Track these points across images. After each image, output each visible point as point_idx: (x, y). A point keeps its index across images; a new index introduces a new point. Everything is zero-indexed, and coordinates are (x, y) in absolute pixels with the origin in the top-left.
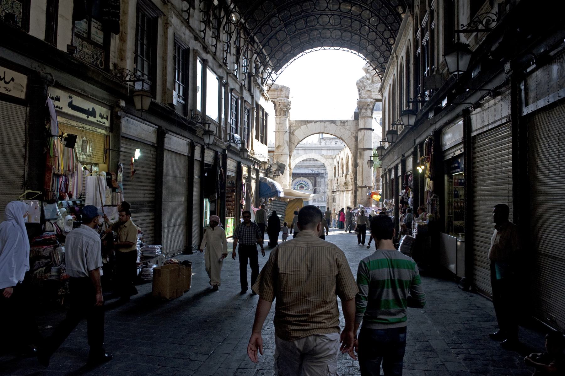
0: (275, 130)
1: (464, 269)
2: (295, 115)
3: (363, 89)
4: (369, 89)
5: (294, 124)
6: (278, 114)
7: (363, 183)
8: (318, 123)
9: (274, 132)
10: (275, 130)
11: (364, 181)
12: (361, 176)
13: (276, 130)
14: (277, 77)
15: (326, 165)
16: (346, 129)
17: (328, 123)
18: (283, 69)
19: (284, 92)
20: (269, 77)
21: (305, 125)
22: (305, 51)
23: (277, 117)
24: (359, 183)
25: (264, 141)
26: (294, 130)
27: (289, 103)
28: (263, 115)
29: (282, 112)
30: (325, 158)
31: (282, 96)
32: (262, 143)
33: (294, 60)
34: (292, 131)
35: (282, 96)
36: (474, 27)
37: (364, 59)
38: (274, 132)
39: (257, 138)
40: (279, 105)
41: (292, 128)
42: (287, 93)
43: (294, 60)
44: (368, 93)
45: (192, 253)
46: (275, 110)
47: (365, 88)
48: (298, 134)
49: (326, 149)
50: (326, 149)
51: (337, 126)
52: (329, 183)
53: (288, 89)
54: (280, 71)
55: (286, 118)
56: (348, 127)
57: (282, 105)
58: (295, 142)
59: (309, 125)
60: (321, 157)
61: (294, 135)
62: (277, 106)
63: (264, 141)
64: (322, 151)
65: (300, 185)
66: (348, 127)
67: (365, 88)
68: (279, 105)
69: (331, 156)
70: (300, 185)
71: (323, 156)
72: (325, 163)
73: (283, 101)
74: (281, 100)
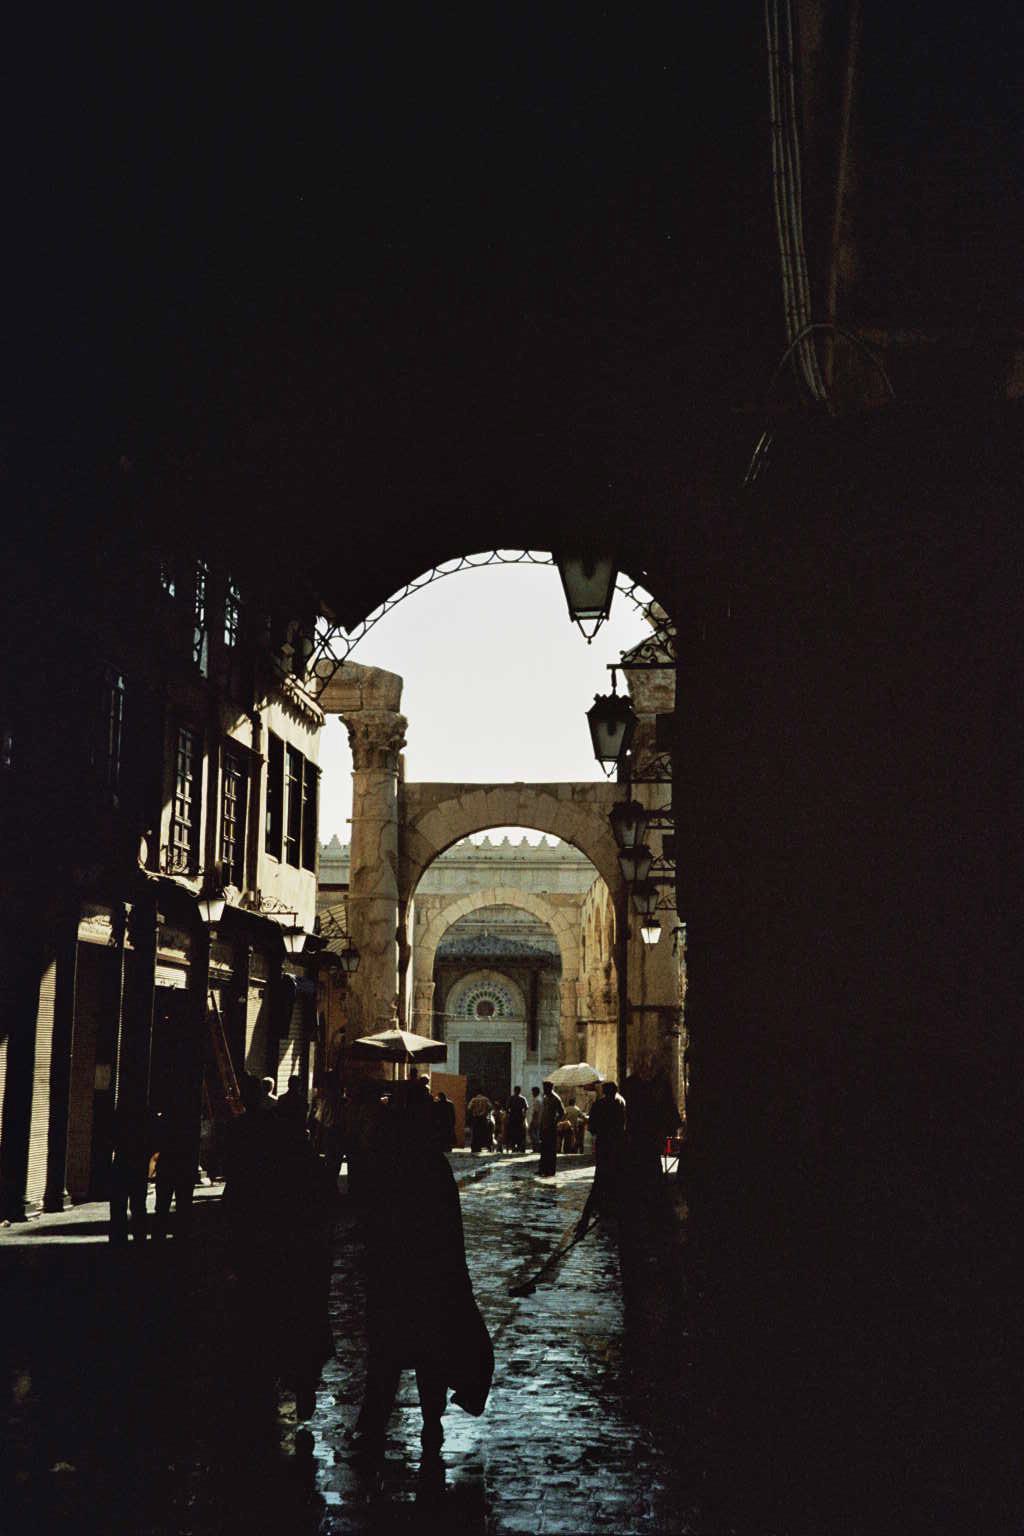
0: (350, 816)
1: (35, 1103)
2: (422, 764)
3: (642, 683)
4: (663, 683)
5: (417, 796)
6: (360, 762)
7: (644, 994)
8: (496, 791)
9: (348, 821)
10: (350, 816)
11: (650, 989)
12: (637, 973)
13: (354, 815)
14: (349, 651)
15: (555, 929)
16: (589, 812)
17: (532, 793)
18: (368, 624)
19: (383, 691)
20: (323, 649)
21: (452, 798)
22: (368, 618)
23: (359, 771)
24: (634, 998)
25: (303, 851)
26: (416, 819)
27: (403, 723)
28: (295, 771)
29: (376, 758)
30: (552, 904)
31: (375, 702)
32: (293, 861)
33: (406, 595)
34: (410, 817)
35: (375, 702)
36: (647, 658)
37: (627, 594)
38: (348, 821)
39: (274, 849)
40: (366, 734)
41: (409, 811)
42: (392, 694)
43: (406, 595)
44: (659, 695)
45: (25, 1219)
46: (350, 751)
47: (648, 678)
48: (432, 827)
49: (575, 866)
50: (575, 866)
51: (561, 801)
52: (566, 995)
53: (396, 683)
54: (360, 628)
55: (389, 778)
56: (595, 807)
57: (374, 734)
58: (419, 855)
59: (466, 799)
60: (539, 900)
61: (415, 831)
62: (359, 735)
63: (303, 851)
64: (560, 874)
65: (478, 1001)
66: (595, 807)
67: (648, 678)
68: (366, 734)
69: (572, 896)
70: (478, 1001)
71: (543, 898)
72: (551, 922)
73: (377, 721)
74: (373, 717)
